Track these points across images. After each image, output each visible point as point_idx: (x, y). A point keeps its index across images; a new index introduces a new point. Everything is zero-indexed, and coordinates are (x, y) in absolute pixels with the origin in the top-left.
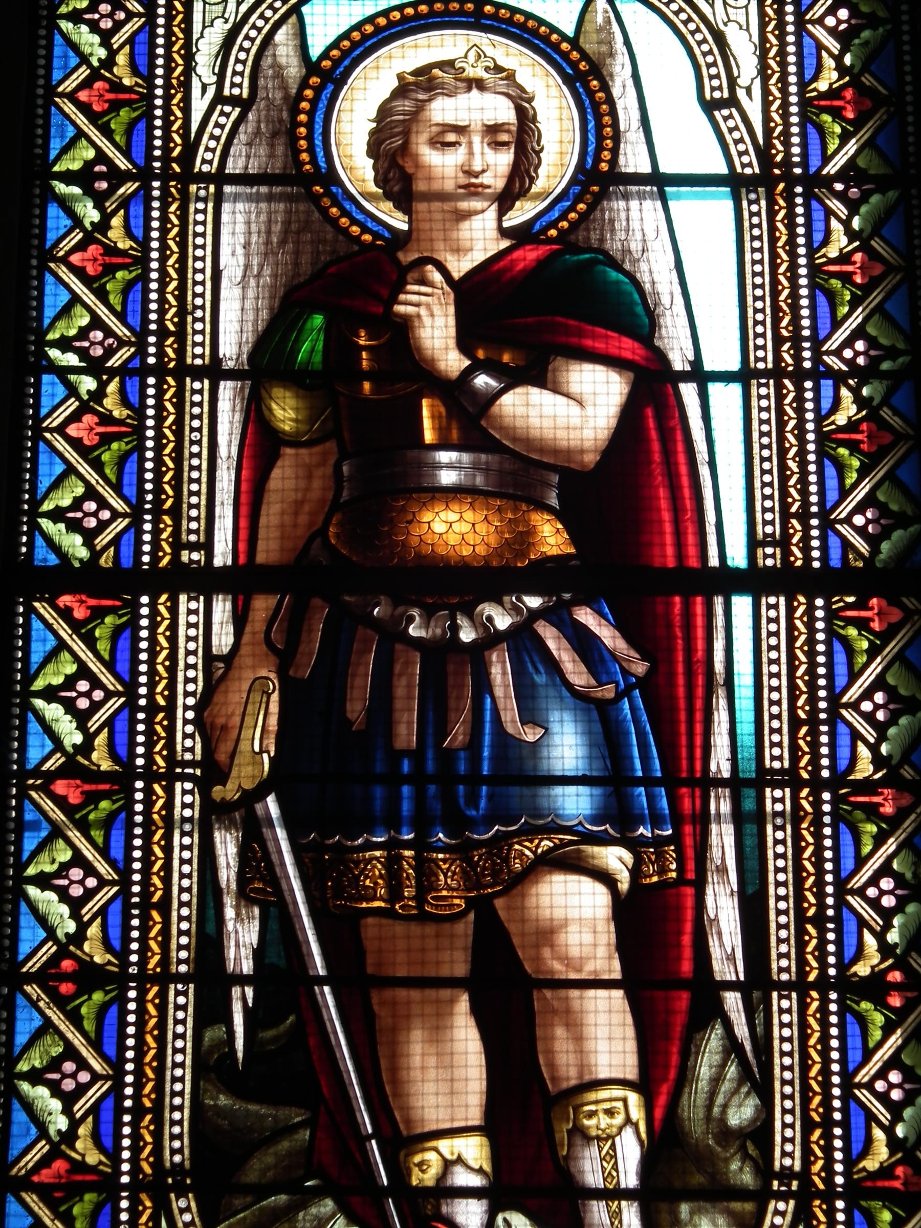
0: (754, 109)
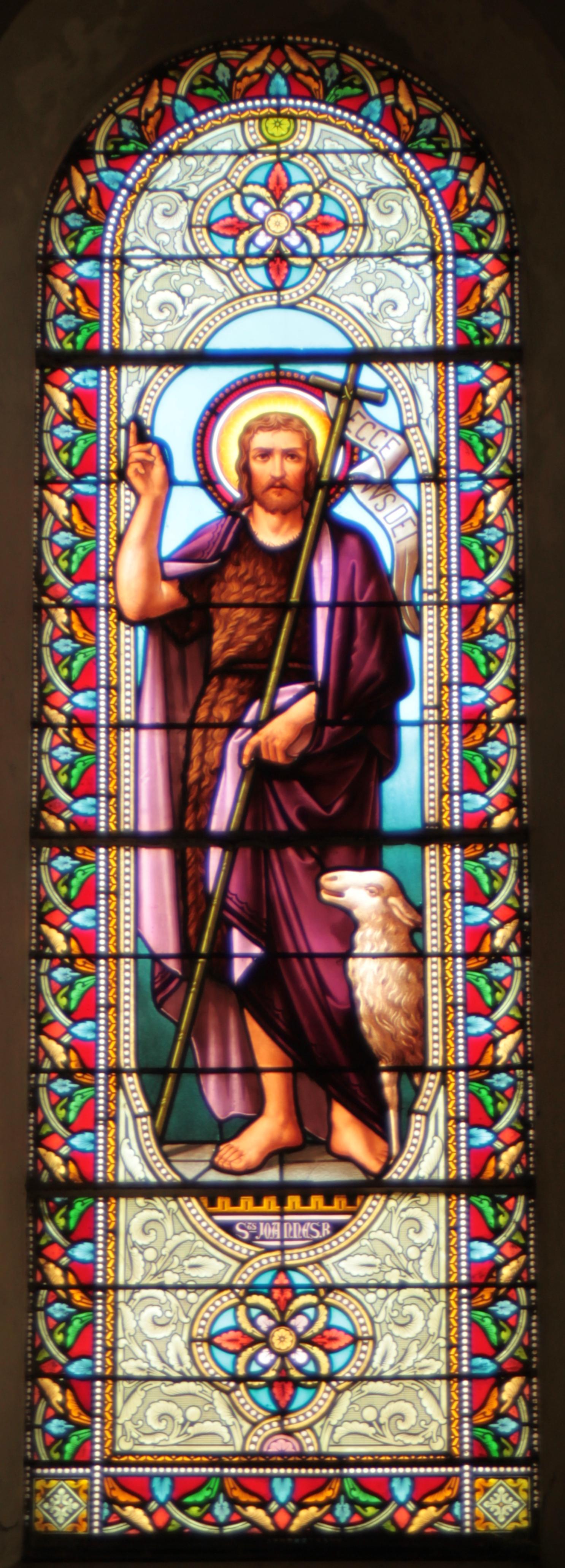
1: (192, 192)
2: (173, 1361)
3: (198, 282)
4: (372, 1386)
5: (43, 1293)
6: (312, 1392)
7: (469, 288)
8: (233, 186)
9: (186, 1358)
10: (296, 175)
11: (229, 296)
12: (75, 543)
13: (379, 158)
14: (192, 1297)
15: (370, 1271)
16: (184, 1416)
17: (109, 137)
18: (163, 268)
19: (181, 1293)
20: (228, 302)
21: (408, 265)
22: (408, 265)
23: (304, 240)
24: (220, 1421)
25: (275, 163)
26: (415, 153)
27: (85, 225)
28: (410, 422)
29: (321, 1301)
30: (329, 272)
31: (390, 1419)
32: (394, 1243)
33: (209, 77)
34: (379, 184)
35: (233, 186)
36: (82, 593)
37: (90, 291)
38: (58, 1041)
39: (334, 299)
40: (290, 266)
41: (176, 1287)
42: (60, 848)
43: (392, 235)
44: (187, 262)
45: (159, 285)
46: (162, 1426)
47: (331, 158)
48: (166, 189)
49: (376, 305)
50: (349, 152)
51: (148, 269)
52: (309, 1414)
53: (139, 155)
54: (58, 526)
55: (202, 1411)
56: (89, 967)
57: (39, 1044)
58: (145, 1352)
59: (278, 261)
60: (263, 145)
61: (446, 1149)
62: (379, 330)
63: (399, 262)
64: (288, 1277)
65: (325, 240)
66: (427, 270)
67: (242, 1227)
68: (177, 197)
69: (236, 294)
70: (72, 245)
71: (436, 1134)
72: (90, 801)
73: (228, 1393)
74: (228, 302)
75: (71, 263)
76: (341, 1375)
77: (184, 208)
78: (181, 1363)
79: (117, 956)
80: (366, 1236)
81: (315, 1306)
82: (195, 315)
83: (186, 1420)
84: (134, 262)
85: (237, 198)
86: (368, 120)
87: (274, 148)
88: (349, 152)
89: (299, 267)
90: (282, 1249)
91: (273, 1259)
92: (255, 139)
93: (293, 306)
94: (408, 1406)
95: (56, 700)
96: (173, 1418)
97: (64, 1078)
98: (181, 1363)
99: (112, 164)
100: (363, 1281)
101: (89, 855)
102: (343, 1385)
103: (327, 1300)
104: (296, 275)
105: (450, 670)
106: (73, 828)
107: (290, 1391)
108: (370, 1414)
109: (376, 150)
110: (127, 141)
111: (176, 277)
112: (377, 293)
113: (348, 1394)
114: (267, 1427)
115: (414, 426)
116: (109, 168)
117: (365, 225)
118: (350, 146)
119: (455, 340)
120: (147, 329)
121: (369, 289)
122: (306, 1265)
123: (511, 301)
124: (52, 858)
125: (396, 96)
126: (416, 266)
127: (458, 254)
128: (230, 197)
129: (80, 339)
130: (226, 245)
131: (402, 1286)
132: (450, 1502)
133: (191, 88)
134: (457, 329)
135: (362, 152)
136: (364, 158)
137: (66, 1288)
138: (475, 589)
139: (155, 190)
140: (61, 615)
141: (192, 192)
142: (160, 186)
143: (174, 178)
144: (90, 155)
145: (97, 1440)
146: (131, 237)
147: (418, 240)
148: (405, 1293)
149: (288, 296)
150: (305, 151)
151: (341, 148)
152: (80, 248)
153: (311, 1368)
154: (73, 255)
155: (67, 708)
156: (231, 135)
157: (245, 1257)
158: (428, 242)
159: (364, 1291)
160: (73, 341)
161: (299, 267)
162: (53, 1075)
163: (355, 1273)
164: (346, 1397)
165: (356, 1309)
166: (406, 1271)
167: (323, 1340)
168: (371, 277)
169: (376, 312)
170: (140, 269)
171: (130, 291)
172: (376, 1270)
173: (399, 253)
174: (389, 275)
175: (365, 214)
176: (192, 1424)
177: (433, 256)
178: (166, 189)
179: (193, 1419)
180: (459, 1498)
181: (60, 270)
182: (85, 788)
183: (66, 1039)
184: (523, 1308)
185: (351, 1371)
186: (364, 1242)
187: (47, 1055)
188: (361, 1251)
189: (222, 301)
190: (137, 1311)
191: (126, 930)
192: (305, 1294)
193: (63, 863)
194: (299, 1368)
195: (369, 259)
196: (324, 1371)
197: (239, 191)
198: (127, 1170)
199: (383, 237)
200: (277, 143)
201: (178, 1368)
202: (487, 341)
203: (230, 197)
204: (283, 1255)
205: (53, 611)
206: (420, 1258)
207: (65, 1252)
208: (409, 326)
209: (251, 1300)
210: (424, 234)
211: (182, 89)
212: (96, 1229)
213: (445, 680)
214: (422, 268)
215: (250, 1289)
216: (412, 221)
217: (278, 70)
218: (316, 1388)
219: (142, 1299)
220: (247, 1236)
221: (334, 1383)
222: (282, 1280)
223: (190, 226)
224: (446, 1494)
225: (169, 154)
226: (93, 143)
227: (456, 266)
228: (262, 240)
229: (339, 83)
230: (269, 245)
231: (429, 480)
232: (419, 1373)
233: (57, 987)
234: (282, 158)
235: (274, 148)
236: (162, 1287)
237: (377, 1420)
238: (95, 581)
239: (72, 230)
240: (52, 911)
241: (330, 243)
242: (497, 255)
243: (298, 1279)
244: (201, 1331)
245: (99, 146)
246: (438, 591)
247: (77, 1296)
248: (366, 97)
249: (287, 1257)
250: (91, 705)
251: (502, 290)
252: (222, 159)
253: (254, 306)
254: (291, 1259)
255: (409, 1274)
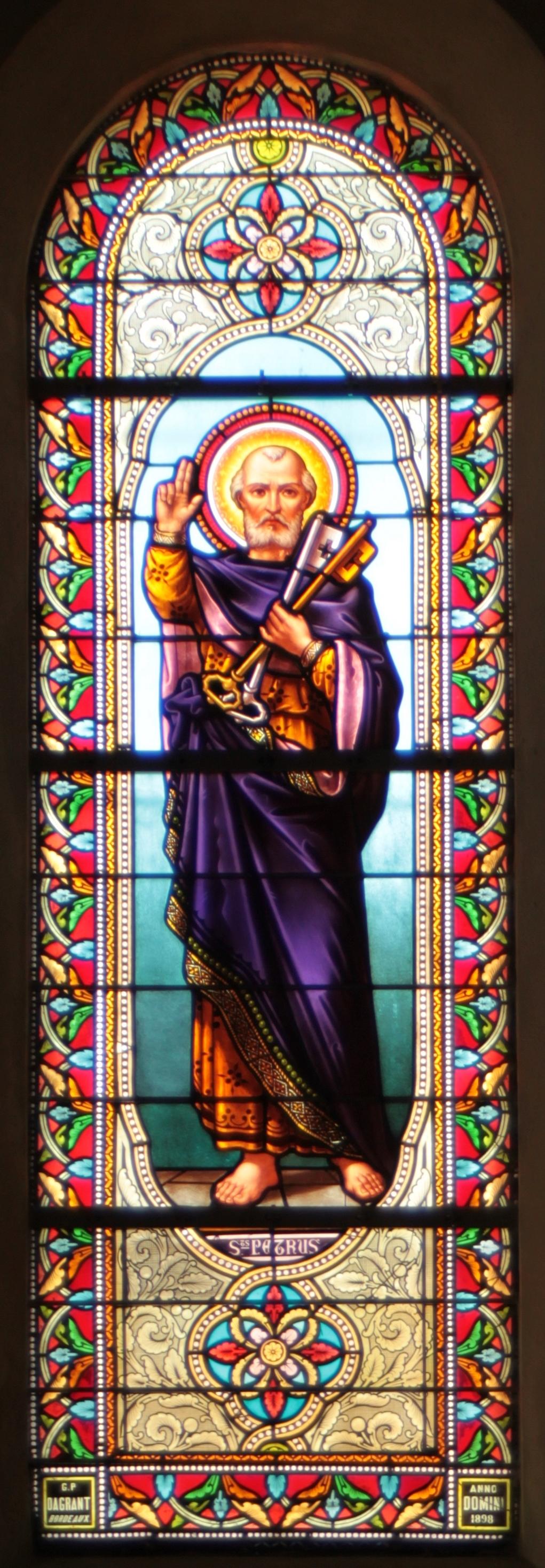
0: (422, 464)
1: (186, 215)
2: (171, 1375)
3: (190, 309)
4: (361, 1398)
5: (47, 881)
6: (302, 1401)
7: (463, 314)
8: (227, 209)
9: (183, 1372)
10: (288, 198)
11: (221, 325)
12: (73, 679)
13: (373, 181)
14: (187, 1314)
15: (357, 1288)
16: (182, 1427)
17: (100, 161)
18: (157, 293)
19: (177, 1309)
20: (220, 330)
21: (401, 292)
22: (401, 292)
23: (298, 265)
24: (216, 1430)
25: (266, 185)
26: (408, 174)
27: (79, 250)
28: (403, 455)
29: (312, 1315)
30: (323, 298)
31: (377, 1429)
32: (382, 1262)
33: (200, 99)
34: (372, 208)
35: (227, 209)
36: (80, 621)
37: (84, 318)
38: (59, 960)
39: (327, 327)
40: (282, 291)
41: (173, 1303)
42: (58, 1230)
43: (385, 261)
44: (180, 288)
45: (151, 311)
46: (160, 1437)
47: (327, 181)
48: (159, 212)
49: (370, 333)
50: (344, 175)
51: (141, 293)
52: (298, 1424)
53: (131, 177)
54: (55, 663)
55: (199, 1422)
56: (87, 998)
57: (40, 963)
58: (144, 1366)
59: (272, 284)
60: (254, 168)
61: (434, 1182)
62: (372, 360)
63: (392, 288)
64: (280, 1291)
65: (318, 265)
66: (420, 296)
67: (235, 1244)
68: (171, 220)
69: (228, 322)
70: (65, 270)
71: (424, 1166)
72: (88, 615)
73: (222, 1404)
74: (220, 330)
75: (64, 288)
76: (329, 1385)
77: (178, 231)
78: (178, 1377)
79: (116, 877)
80: (354, 1254)
81: (306, 1320)
82: (187, 343)
83: (184, 1431)
84: (128, 287)
85: (231, 221)
86: (360, 140)
87: (265, 170)
88: (344, 175)
89: (293, 293)
90: (274, 1265)
91: (264, 1275)
92: (248, 162)
93: (285, 334)
94: (396, 1417)
95: (53, 950)
96: (172, 1429)
97: (63, 1105)
98: (178, 1377)
99: (105, 188)
100: (351, 1297)
101: (86, 780)
102: (331, 1396)
103: (318, 1314)
104: (288, 301)
105: (441, 706)
106: (71, 749)
107: (280, 1401)
108: (358, 1424)
109: (369, 173)
110: (119, 165)
111: (168, 304)
112: (371, 320)
113: (337, 1406)
114: (261, 1435)
115: (406, 459)
116: (102, 192)
117: (359, 249)
118: (342, 169)
119: (449, 368)
120: (141, 358)
121: (363, 317)
122: (297, 1280)
123: (504, 331)
124: (52, 783)
125: (388, 116)
126: (410, 292)
127: (451, 280)
128: (224, 220)
129: (72, 369)
130: (218, 270)
131: (389, 1302)
132: (435, 1500)
133: (182, 109)
134: (451, 358)
135: (355, 174)
136: (357, 181)
137: (69, 876)
138: (464, 619)
139: (149, 212)
140: (59, 647)
141: (186, 215)
142: (154, 208)
143: (168, 200)
144: (85, 178)
145: (99, 1256)
146: (125, 261)
147: (411, 266)
148: (392, 1308)
149: (280, 324)
150: (296, 173)
151: (333, 171)
152: (74, 273)
153: (300, 1379)
154: (66, 279)
155: (66, 737)
156: (224, 158)
157: (236, 1274)
158: (421, 268)
159: (354, 1306)
160: (65, 369)
161: (293, 293)
162: (52, 1104)
163: (343, 1290)
164: (336, 1408)
165: (344, 1324)
166: (393, 1288)
167: (313, 1353)
168: (364, 305)
169: (370, 340)
170: (132, 294)
171: (123, 317)
172: (364, 1287)
173: (393, 279)
174: (382, 302)
175: (358, 239)
176: (190, 1435)
177: (425, 282)
178: (159, 212)
179: (191, 1430)
180: (443, 1495)
181: (52, 295)
182: (85, 708)
183: (66, 958)
184: (508, 1356)
185: (338, 1382)
186: (353, 1260)
187: (49, 975)
188: (350, 1268)
189: (215, 328)
190: (135, 1327)
191: (124, 932)
192: (295, 1308)
193: (62, 788)
194: (289, 1379)
195: (362, 286)
196: (313, 1381)
197: (233, 214)
198: (124, 1199)
199: (377, 262)
200: (269, 166)
201: (175, 1381)
202: (481, 372)
203: (224, 220)
204: (274, 1271)
205: (52, 643)
206: (406, 1275)
207: (66, 1168)
208: (403, 355)
209: (244, 1313)
210: (418, 260)
211: (173, 111)
212: (95, 1279)
213: (435, 716)
214: (415, 294)
215: (244, 1303)
216: (406, 245)
217: (269, 91)
218: (307, 1398)
219: (140, 1316)
220: (238, 1253)
221: (322, 1395)
222: (275, 1294)
223: (184, 250)
224: (431, 1491)
225: (161, 177)
226: (85, 167)
227: (449, 292)
228: (254, 266)
229: (332, 103)
230: (260, 271)
231: (422, 516)
232: (406, 1385)
233: (57, 908)
234: (274, 182)
235: (265, 170)
236: (158, 1303)
237: (365, 1431)
238: (93, 610)
239: (66, 254)
240: (51, 943)
241: (323, 268)
242: (489, 282)
243: (290, 1295)
244: (196, 1344)
245: (92, 169)
246: (429, 627)
247: (78, 882)
248: (360, 117)
249: (278, 1273)
250: (88, 1174)
251: (494, 318)
252: (215, 181)
253: (244, 335)
254: (283, 1274)
255: (396, 1291)
